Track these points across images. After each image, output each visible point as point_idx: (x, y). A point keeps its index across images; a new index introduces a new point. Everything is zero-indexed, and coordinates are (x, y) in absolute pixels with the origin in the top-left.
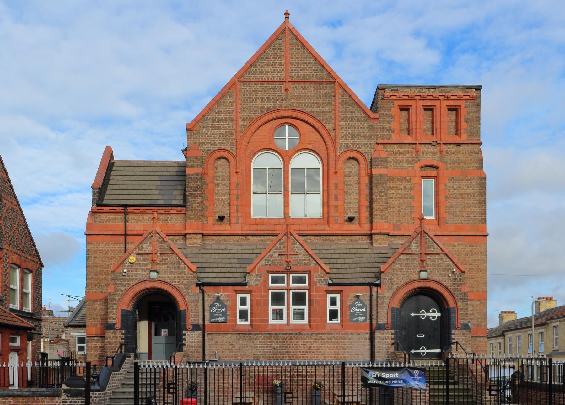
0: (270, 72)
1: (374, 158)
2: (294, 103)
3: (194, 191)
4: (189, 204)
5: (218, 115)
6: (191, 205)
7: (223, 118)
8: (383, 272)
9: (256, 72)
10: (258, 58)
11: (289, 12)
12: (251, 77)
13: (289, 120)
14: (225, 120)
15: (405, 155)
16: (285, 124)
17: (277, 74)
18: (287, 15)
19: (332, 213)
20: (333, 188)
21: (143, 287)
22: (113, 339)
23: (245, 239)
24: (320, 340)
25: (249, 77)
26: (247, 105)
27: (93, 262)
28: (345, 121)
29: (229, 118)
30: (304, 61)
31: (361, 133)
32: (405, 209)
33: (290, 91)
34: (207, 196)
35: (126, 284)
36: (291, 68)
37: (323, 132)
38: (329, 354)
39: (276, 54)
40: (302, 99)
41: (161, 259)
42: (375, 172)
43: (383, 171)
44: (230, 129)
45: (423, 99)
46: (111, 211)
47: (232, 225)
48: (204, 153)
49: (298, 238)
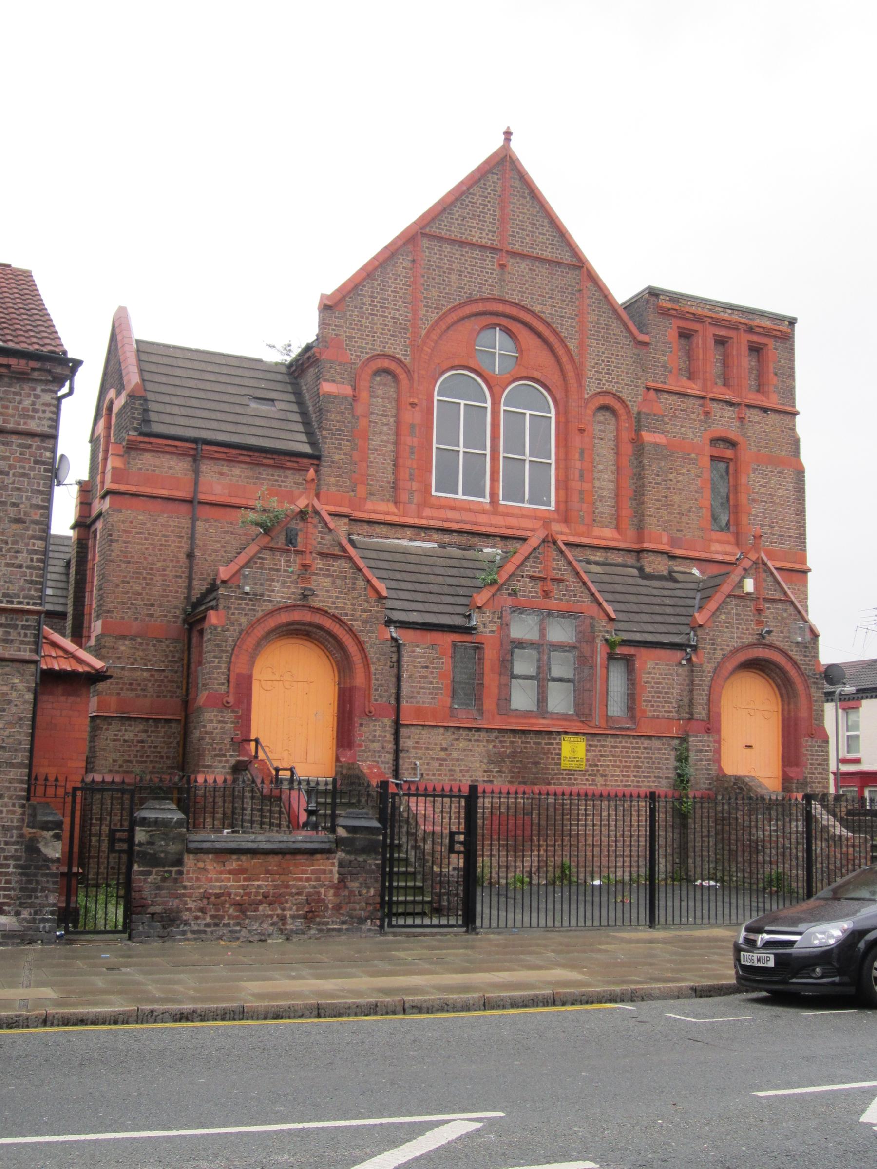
0: (474, 228)
1: (645, 413)
2: (514, 290)
3: (337, 430)
4: (326, 453)
5: (381, 289)
6: (331, 457)
7: (390, 296)
8: (701, 626)
9: (451, 223)
10: (457, 199)
11: (512, 130)
12: (443, 229)
13: (504, 321)
14: (394, 301)
15: (688, 415)
16: (493, 326)
17: (487, 234)
18: (508, 134)
19: (575, 504)
20: (577, 456)
21: (284, 621)
22: (217, 728)
23: (423, 535)
24: (599, 748)
25: (440, 229)
26: (434, 279)
27: (121, 551)
28: (596, 340)
29: (401, 297)
30: (533, 220)
31: (622, 364)
32: (690, 511)
33: (509, 268)
34: (356, 442)
35: (250, 610)
36: (511, 227)
37: (561, 352)
38: (613, 776)
39: (486, 197)
40: (527, 286)
41: (320, 566)
42: (648, 437)
43: (659, 439)
44: (403, 320)
45: (750, 330)
46: (167, 449)
47: (401, 506)
48: (353, 357)
49: (563, 548)
